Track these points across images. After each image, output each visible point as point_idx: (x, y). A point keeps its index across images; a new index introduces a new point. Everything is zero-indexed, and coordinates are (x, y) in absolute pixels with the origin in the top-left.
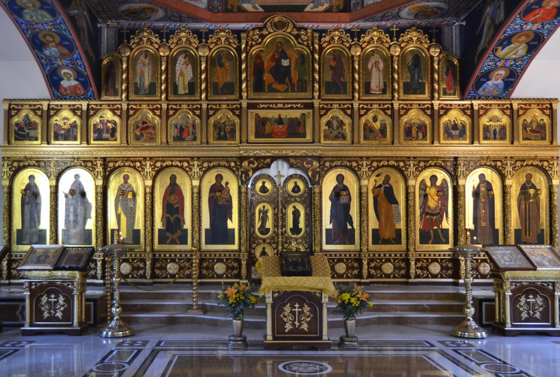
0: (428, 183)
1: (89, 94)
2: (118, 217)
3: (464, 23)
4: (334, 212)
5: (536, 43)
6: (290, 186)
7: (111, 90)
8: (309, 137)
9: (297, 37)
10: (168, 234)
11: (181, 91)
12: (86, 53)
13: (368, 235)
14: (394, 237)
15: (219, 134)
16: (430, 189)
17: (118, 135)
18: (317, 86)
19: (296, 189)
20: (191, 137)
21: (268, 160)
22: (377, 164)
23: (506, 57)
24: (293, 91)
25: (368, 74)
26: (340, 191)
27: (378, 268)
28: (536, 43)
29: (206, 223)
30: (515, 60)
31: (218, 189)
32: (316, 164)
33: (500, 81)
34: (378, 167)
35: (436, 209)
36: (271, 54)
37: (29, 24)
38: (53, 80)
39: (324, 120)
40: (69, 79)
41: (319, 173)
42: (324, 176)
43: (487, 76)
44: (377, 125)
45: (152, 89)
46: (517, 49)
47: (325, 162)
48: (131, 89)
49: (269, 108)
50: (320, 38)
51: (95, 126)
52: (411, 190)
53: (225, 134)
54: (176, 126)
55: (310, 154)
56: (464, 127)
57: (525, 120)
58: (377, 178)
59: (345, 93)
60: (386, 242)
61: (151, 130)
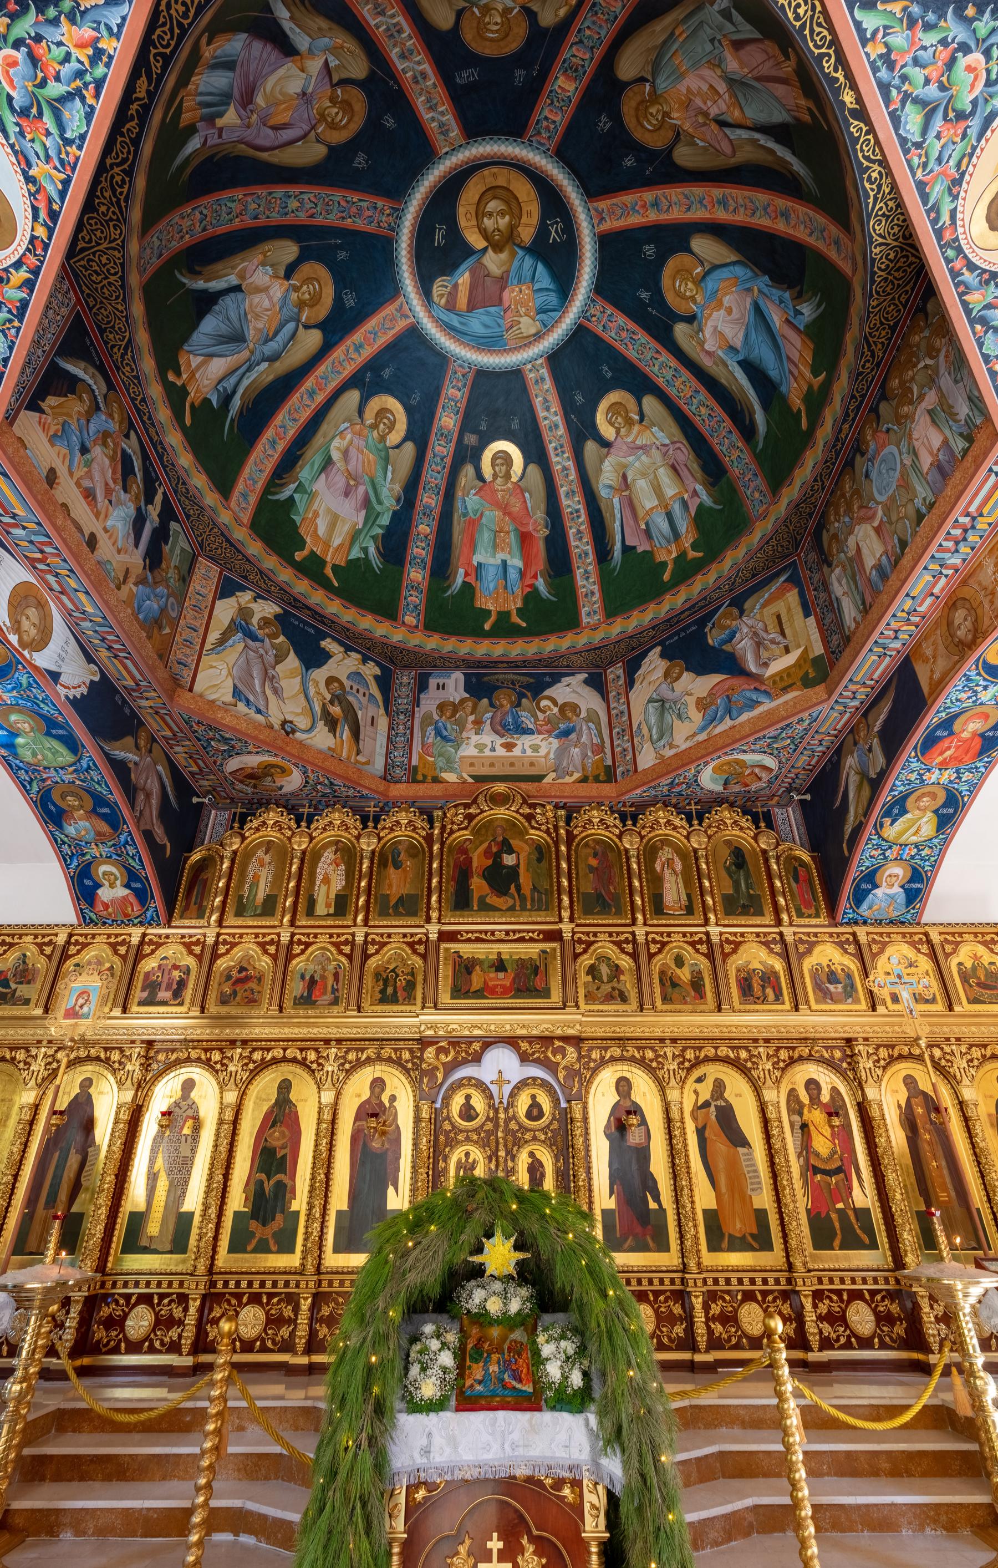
0: (804, 1097)
1: (149, 914)
2: (152, 1178)
3: (808, 797)
4: (616, 1166)
5: (950, 812)
6: (523, 1103)
7: (193, 907)
8: (556, 997)
9: (529, 817)
10: (254, 1225)
11: (321, 909)
12: (148, 836)
13: (695, 1226)
14: (755, 1231)
15: (383, 991)
17: (188, 994)
18: (566, 900)
19: (535, 1112)
20: (328, 997)
21: (476, 1046)
22: (696, 1054)
23: (902, 841)
24: (523, 908)
25: (656, 881)
26: (624, 1119)
27: (729, 1319)
28: (951, 811)
29: (340, 1200)
30: (917, 846)
31: (374, 1112)
32: (571, 1052)
33: (897, 890)
34: (697, 1063)
35: (831, 1157)
36: (485, 845)
37: (33, 769)
38: (84, 887)
39: (586, 961)
40: (112, 886)
41: (578, 1073)
42: (590, 1082)
43: (871, 878)
44: (684, 975)
45: (269, 907)
46: (917, 825)
47: (591, 1049)
48: (230, 909)
49: (478, 940)
50: (568, 820)
51: (147, 975)
52: (772, 1114)
53: (395, 992)
54: (303, 977)
55: (559, 1032)
56: (849, 976)
57: (960, 964)
58: (698, 1086)
59: (619, 913)
61: (252, 985)
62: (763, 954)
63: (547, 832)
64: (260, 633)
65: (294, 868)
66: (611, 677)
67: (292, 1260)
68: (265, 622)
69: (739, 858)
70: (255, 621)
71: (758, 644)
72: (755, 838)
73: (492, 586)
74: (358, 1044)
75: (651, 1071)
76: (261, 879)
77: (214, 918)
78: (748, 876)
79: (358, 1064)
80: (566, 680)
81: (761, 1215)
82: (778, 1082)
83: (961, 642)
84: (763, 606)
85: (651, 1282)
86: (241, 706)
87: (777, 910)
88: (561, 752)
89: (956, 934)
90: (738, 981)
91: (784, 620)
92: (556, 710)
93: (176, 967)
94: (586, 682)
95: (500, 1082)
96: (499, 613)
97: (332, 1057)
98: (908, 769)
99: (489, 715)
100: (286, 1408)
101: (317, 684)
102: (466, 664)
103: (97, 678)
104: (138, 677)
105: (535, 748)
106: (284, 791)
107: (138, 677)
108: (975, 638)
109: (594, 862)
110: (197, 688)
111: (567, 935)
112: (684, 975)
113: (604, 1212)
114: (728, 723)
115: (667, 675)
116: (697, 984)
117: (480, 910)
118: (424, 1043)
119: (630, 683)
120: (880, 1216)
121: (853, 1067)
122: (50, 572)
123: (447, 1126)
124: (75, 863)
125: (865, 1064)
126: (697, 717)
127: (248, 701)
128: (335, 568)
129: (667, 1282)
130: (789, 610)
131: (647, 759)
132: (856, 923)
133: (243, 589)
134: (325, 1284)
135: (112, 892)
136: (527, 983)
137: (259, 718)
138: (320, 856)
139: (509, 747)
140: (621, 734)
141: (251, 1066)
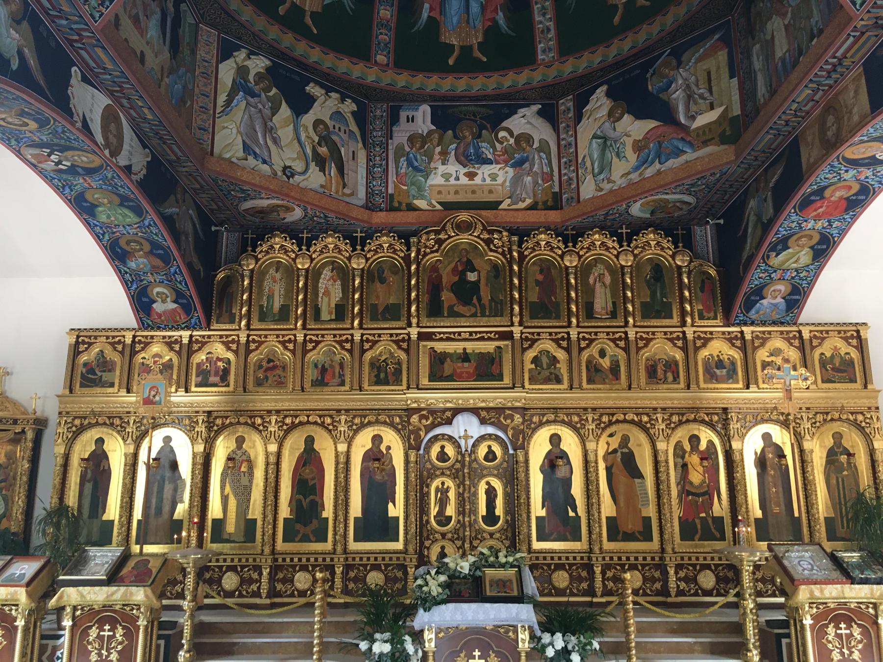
0: (687, 447)
1: (193, 321)
3: (722, 221)
5: (823, 249)
6: (482, 451)
8: (507, 380)
9: (488, 242)
10: (298, 526)
11: (325, 316)
12: (190, 266)
13: (600, 526)
14: (641, 530)
16: (690, 456)
18: (516, 308)
19: (491, 456)
20: (337, 380)
21: (449, 414)
22: (608, 418)
23: (784, 267)
25: (589, 292)
26: (555, 460)
28: (825, 247)
30: (796, 270)
31: (376, 457)
34: (611, 423)
38: (141, 302)
39: (531, 354)
41: (522, 431)
42: (531, 437)
43: (759, 293)
44: (606, 363)
45: (284, 315)
46: (799, 256)
47: (532, 416)
49: (449, 339)
51: (198, 365)
52: (661, 458)
54: (316, 366)
55: (509, 405)
56: (733, 363)
57: (822, 354)
58: (610, 439)
59: (558, 317)
60: (629, 537)
61: (279, 372)
62: (668, 347)
63: (503, 254)
64: (256, 89)
65: (301, 284)
66: (562, 108)
67: (328, 546)
68: (259, 76)
69: (658, 270)
70: (251, 78)
71: (689, 97)
72: (673, 257)
73: (455, 20)
74: (362, 413)
75: (576, 430)
76: (275, 291)
77: (243, 323)
78: (663, 287)
79: (363, 426)
80: (522, 111)
81: (647, 521)
82: (668, 437)
83: (828, 140)
84: (698, 60)
85: (567, 558)
86: (250, 158)
87: (683, 314)
88: (516, 181)
89: (823, 332)
90: (647, 368)
91: (713, 77)
92: (512, 141)
93: (219, 359)
94: (540, 113)
95: (466, 437)
96: (462, 47)
97: (343, 422)
98: (789, 220)
99: (454, 146)
100: (339, 622)
101: (306, 128)
102: (431, 98)
103: (149, 159)
104: (180, 154)
105: (494, 177)
106: (286, 221)
107: (180, 154)
108: (836, 143)
109: (540, 278)
110: (216, 150)
111: (517, 336)
112: (606, 363)
113: (538, 518)
114: (657, 165)
115: (610, 114)
116: (615, 370)
117: (449, 316)
118: (410, 411)
119: (579, 118)
120: (730, 521)
121: (726, 426)
122: (124, 97)
123: (428, 466)
124: (135, 286)
125: (734, 426)
126: (632, 157)
127: (255, 153)
128: (314, 15)
129: (578, 558)
130: (718, 68)
131: (588, 190)
132: (745, 324)
133: (238, 48)
134: (350, 559)
135: (164, 306)
136: (486, 370)
137: (265, 167)
138: (320, 274)
139: (471, 176)
140: (568, 164)
141: (285, 427)
